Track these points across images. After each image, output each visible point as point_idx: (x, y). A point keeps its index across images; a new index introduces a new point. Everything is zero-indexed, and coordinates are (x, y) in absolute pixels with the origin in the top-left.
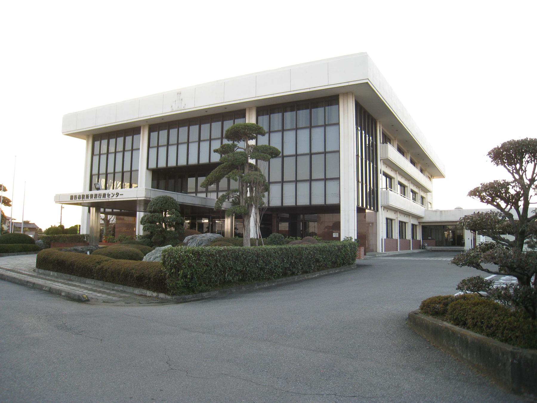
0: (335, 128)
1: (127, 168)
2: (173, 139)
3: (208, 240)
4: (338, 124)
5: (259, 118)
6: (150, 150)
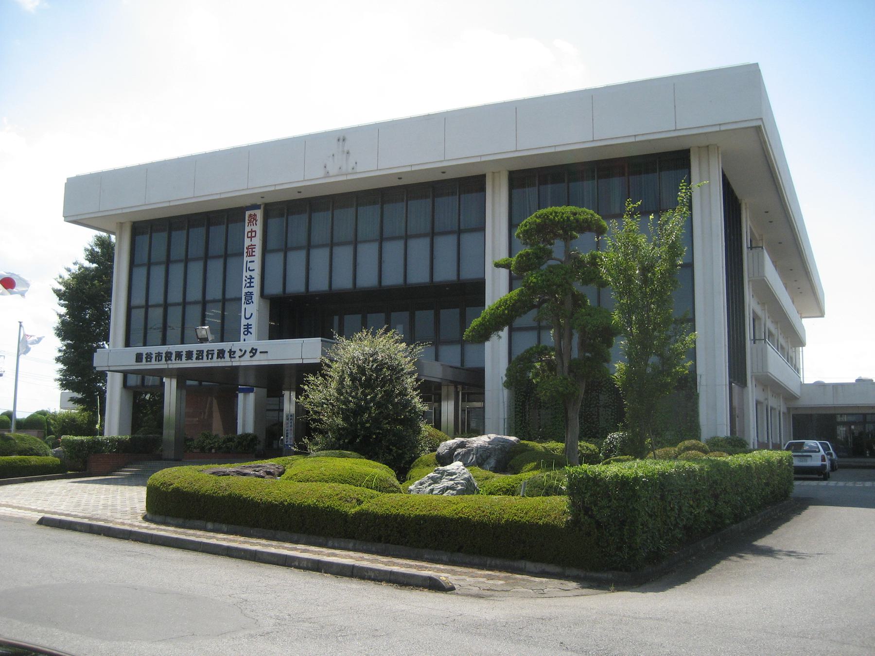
0: (477, 235)
1: (214, 293)
2: (178, 251)
3: (501, 449)
4: (482, 229)
5: (514, 191)
6: (135, 270)
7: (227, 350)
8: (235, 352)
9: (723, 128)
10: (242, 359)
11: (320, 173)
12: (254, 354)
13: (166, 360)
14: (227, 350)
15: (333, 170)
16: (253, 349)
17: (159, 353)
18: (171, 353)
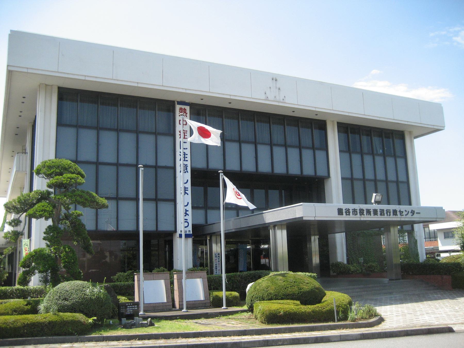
7: (398, 210)
8: (402, 212)
9: (30, 71)
10: (407, 216)
11: (263, 97)
12: (413, 214)
13: (360, 215)
14: (398, 210)
15: (271, 97)
16: (412, 211)
17: (354, 209)
18: (349, 209)
